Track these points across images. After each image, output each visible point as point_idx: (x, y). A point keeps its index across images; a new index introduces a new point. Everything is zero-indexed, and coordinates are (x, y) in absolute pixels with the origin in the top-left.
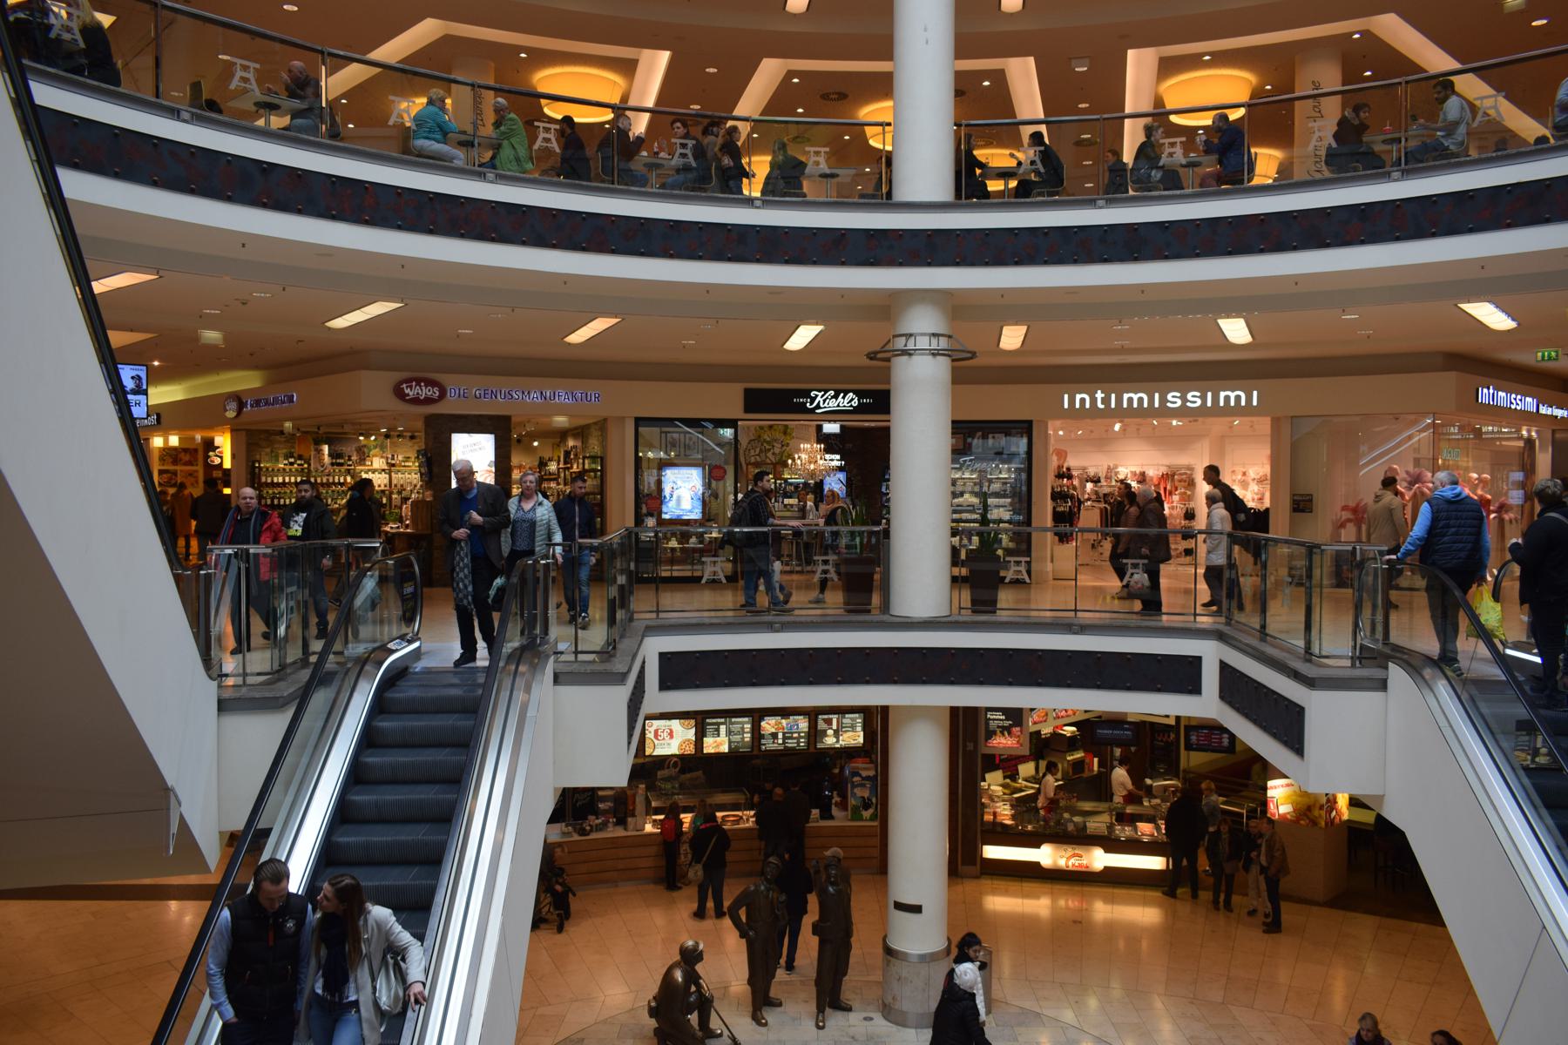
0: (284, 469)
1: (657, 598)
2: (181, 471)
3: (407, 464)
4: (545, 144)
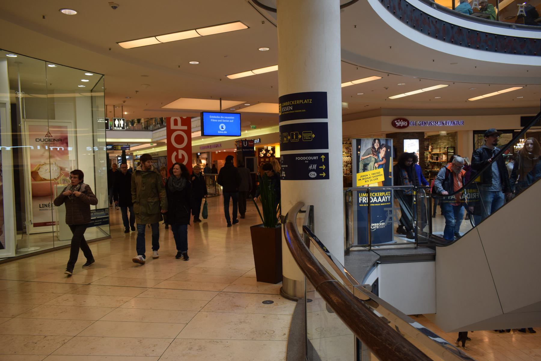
4: (521, 13)
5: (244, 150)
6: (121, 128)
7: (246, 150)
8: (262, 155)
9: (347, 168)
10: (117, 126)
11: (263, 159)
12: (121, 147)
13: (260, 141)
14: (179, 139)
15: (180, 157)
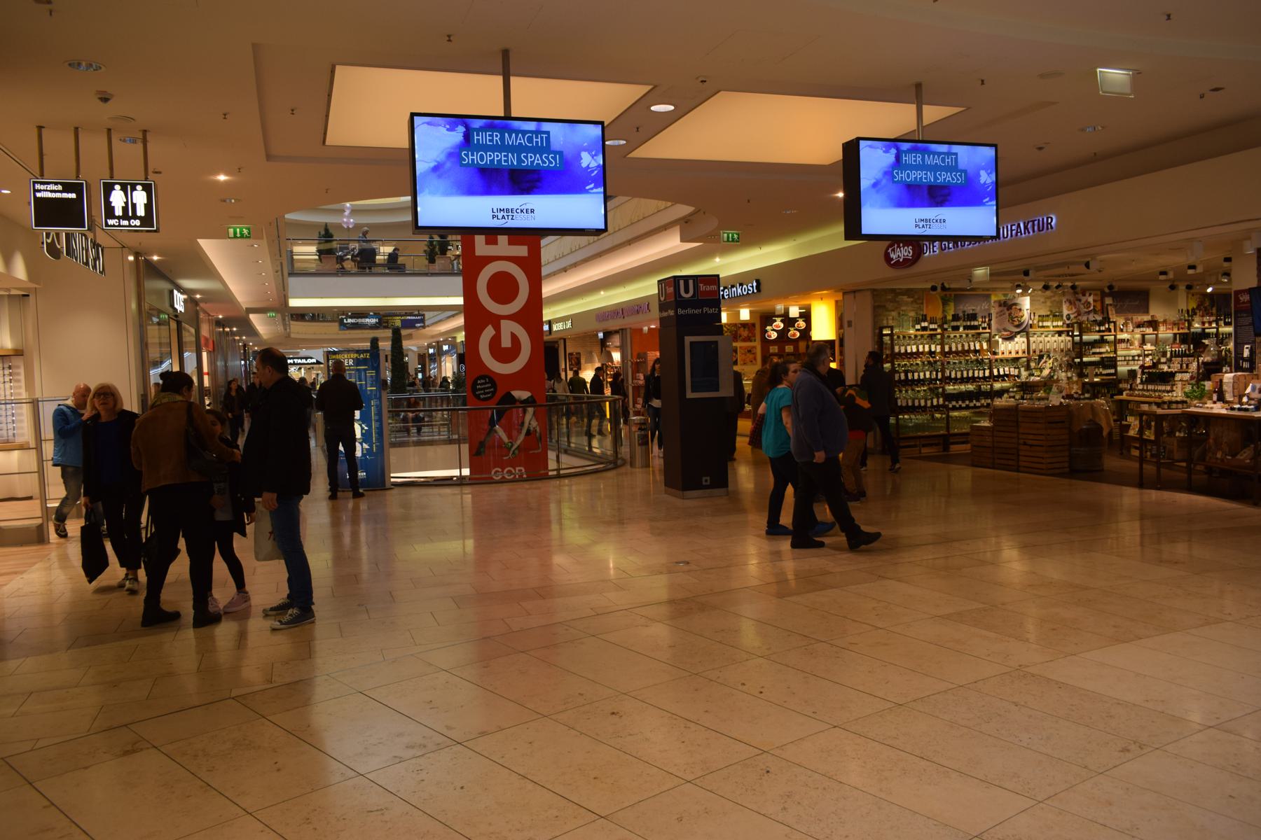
0: (916, 336)
1: (29, 403)
2: (740, 347)
3: (1045, 324)
5: (680, 311)
6: (137, 222)
7: (690, 311)
8: (774, 335)
9: (1069, 374)
10: (119, 212)
11: (776, 347)
12: (402, 320)
13: (758, 287)
14: (503, 288)
15: (506, 342)
